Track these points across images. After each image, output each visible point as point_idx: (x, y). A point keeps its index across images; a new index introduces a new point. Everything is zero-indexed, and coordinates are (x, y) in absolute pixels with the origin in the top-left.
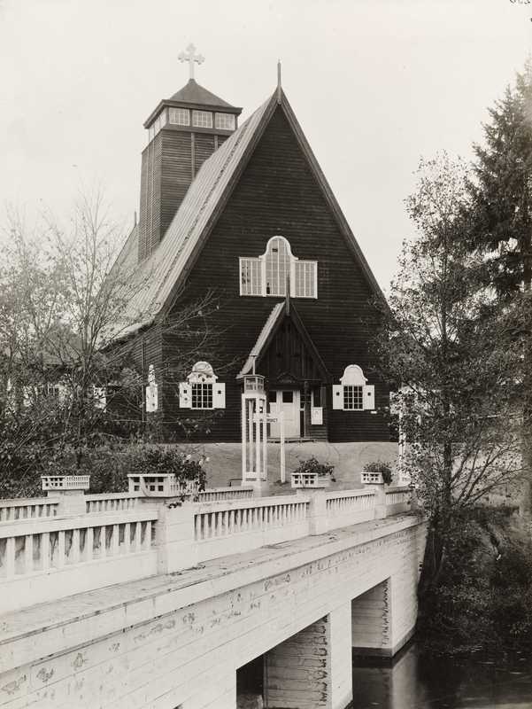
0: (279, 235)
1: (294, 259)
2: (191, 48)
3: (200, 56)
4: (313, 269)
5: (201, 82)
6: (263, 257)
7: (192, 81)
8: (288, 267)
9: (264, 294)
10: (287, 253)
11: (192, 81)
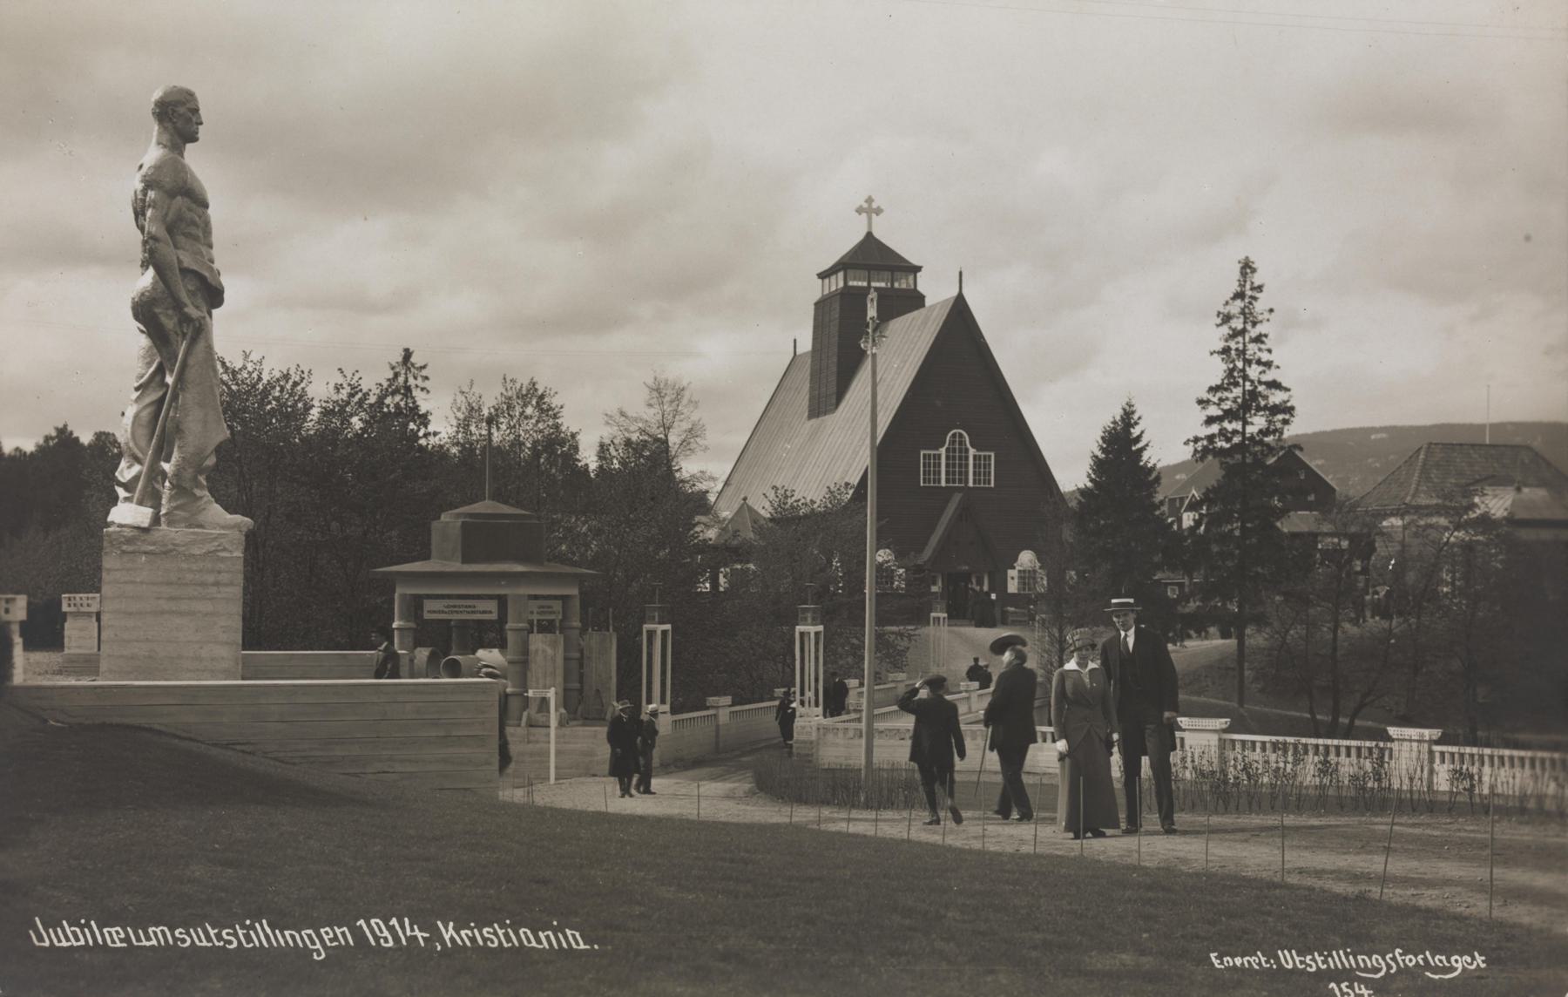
0: (957, 428)
1: (972, 451)
2: (870, 200)
3: (878, 207)
4: (990, 460)
5: (877, 234)
6: (943, 451)
7: (869, 235)
8: (967, 458)
9: (943, 484)
10: (965, 445)
11: (869, 235)
